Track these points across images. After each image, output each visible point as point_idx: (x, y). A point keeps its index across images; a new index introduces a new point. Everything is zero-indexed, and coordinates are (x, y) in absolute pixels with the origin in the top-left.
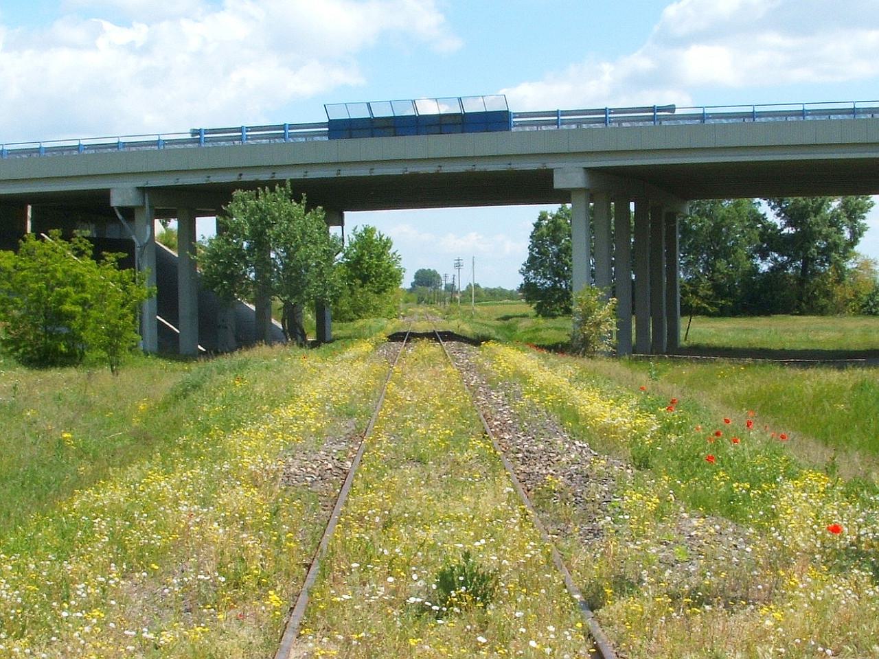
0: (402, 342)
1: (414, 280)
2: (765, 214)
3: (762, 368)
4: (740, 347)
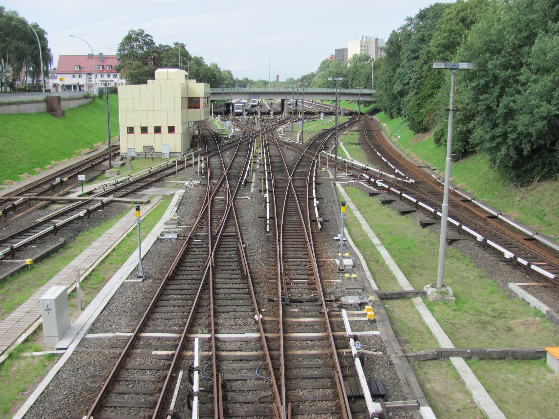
0: (507, 71)
1: (218, 67)
2: (420, 9)
3: (502, 168)
4: (98, 228)
